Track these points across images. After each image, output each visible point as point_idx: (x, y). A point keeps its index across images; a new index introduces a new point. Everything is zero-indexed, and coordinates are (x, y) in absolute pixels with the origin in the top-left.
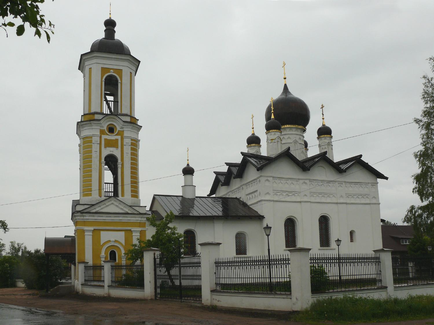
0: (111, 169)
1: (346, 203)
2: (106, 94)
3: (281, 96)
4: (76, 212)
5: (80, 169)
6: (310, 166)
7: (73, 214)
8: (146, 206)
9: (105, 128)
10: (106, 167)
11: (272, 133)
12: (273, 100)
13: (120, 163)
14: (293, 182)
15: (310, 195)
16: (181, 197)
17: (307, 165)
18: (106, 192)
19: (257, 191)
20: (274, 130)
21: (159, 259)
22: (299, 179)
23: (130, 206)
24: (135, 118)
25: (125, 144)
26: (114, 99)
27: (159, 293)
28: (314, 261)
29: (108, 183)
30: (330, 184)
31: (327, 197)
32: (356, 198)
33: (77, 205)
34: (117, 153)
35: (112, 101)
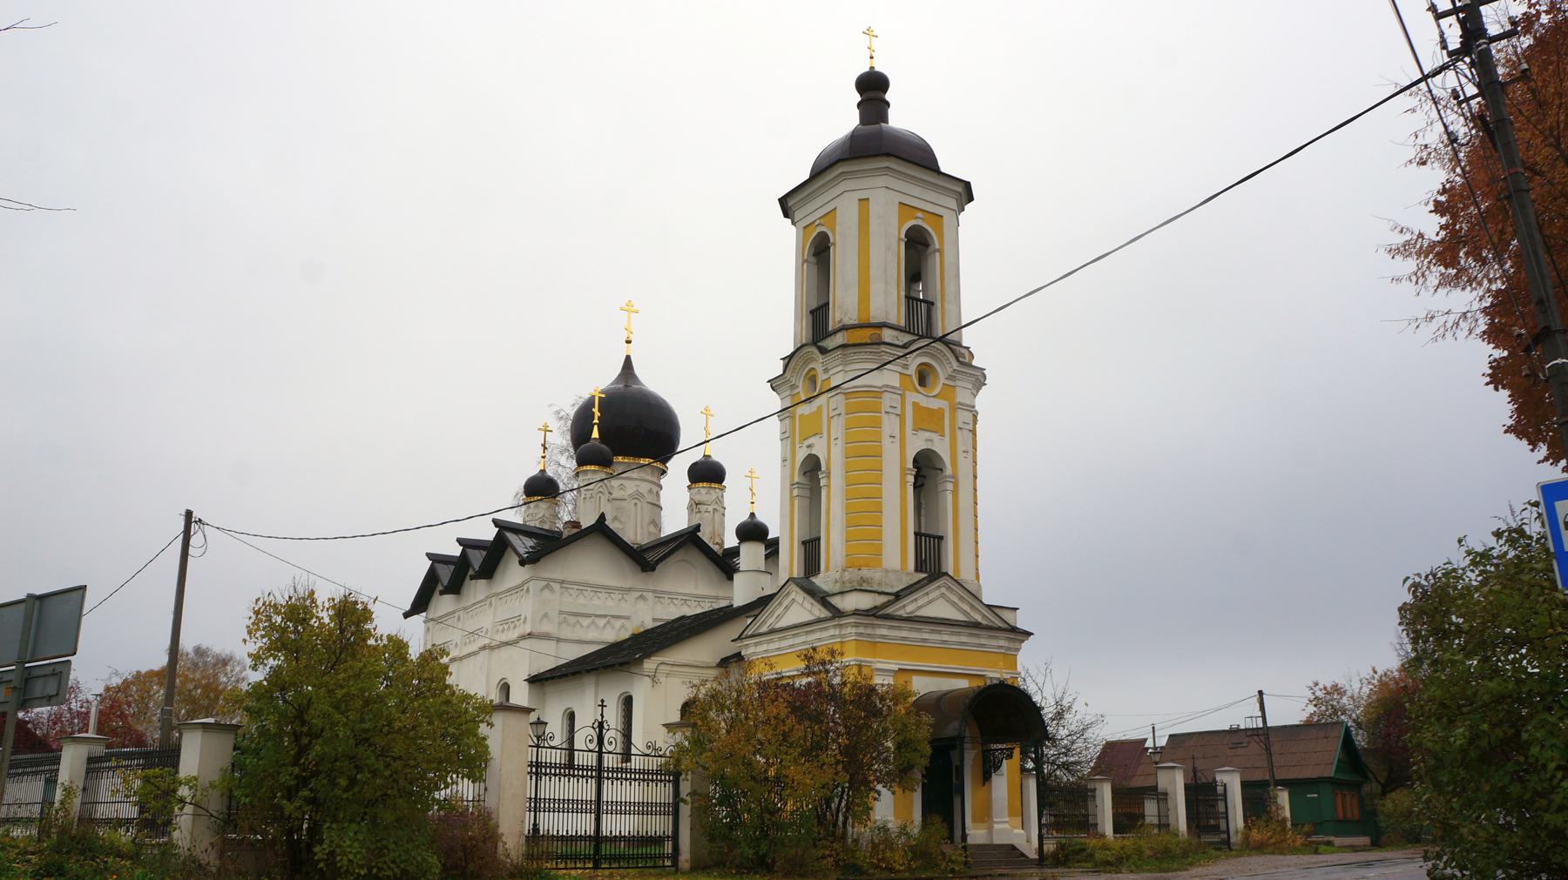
3: (612, 384)
9: (912, 370)
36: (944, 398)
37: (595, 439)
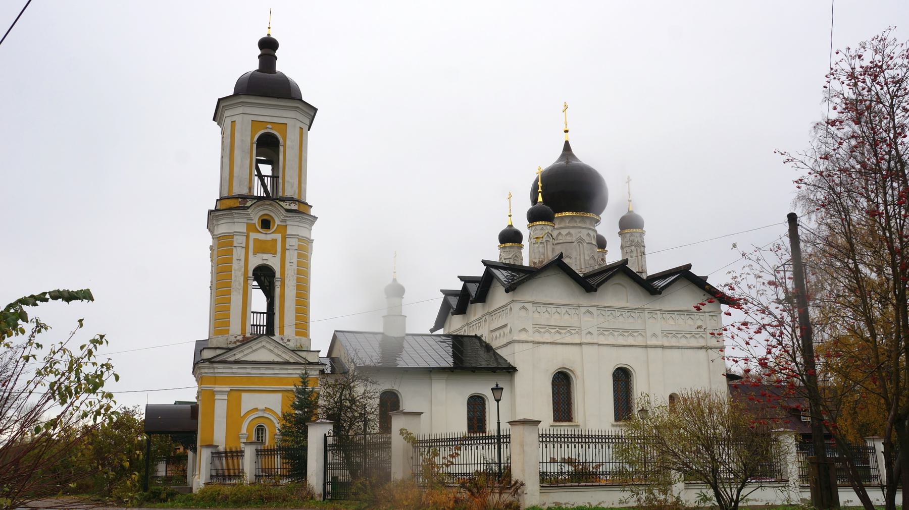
0: (262, 286)
1: (663, 347)
2: (258, 161)
3: (557, 162)
4: (202, 361)
5: (210, 287)
6: (598, 284)
7: (195, 365)
8: (320, 351)
9: (256, 221)
10: (255, 283)
11: (537, 227)
12: (541, 170)
13: (279, 278)
14: (568, 310)
15: (599, 332)
16: (381, 335)
17: (592, 282)
18: (253, 325)
19: (506, 326)
20: (541, 223)
21: (331, 437)
22: (579, 306)
23: (293, 351)
24: (306, 204)
25: (288, 247)
26: (273, 170)
27: (329, 492)
28: (597, 440)
29: (257, 313)
30: (633, 313)
31: (628, 336)
32: (681, 338)
33: (204, 348)
34: (274, 262)
35: (268, 176)
36: (279, 232)
37: (540, 202)
